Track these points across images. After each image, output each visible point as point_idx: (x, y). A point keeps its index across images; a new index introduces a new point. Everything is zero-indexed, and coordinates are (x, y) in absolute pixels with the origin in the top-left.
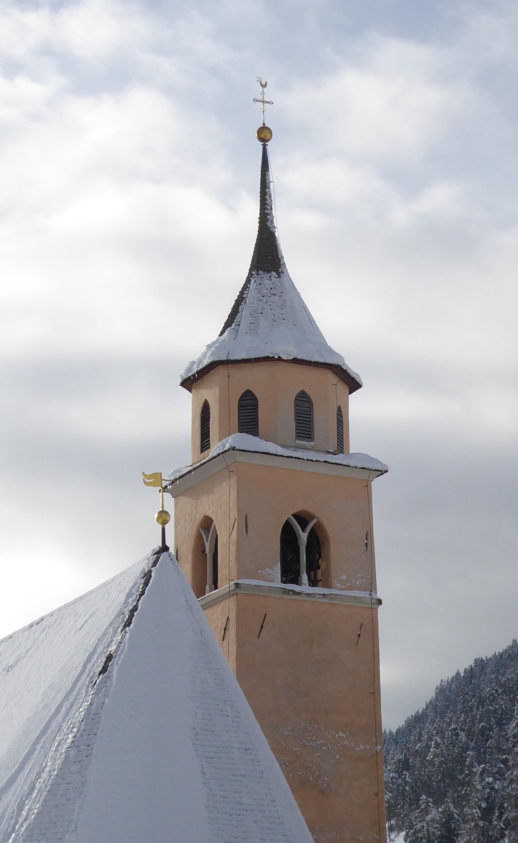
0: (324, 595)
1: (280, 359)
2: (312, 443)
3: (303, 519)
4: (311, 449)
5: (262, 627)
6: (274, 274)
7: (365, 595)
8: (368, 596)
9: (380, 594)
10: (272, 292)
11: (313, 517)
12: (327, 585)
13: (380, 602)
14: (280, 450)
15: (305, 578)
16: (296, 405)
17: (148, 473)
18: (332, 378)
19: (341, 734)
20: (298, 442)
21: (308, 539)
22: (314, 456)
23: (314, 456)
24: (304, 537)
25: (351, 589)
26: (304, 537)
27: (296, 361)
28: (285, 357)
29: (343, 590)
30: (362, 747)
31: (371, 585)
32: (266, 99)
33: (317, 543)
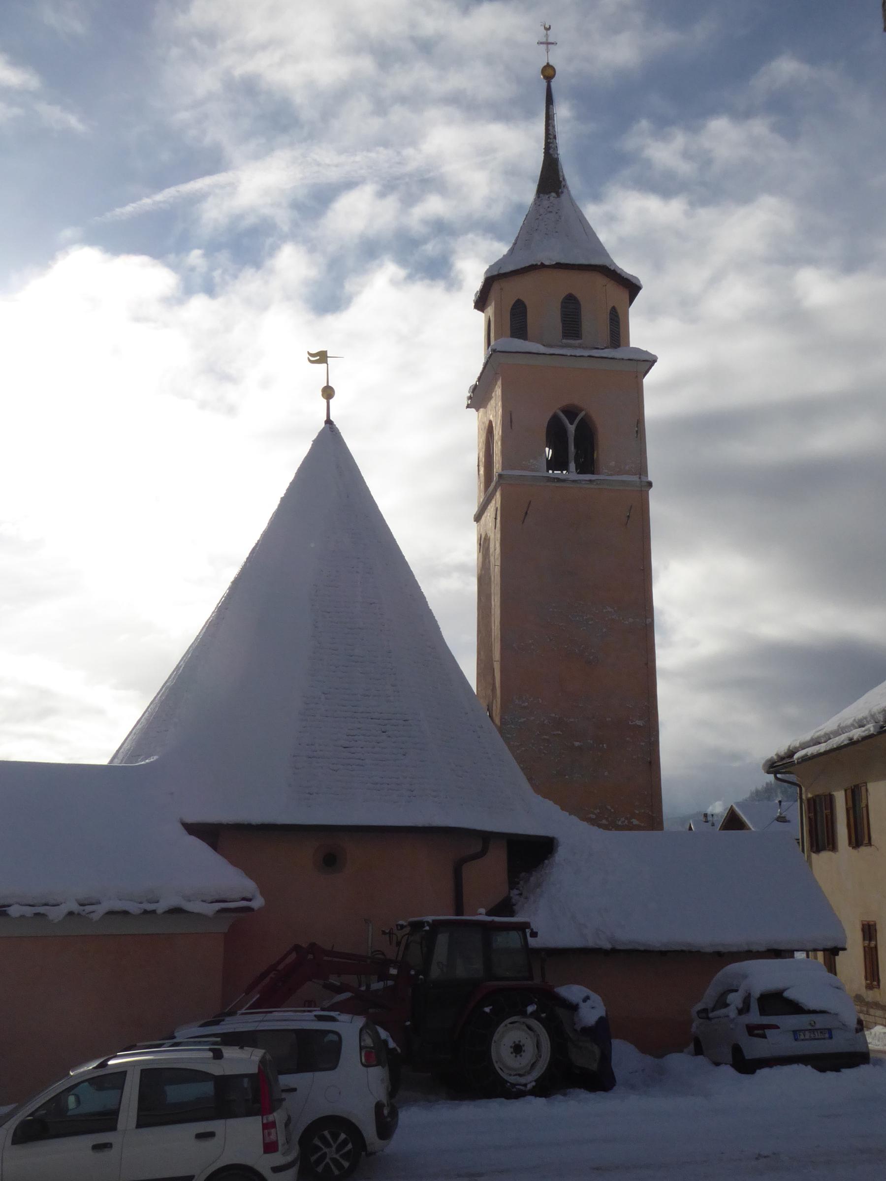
0: (590, 481)
1: (543, 266)
2: (579, 341)
3: (571, 412)
4: (580, 347)
5: (526, 513)
6: (553, 194)
7: (635, 478)
8: (638, 480)
9: (651, 477)
10: (549, 210)
11: (581, 410)
12: (598, 474)
13: (650, 484)
14: (542, 349)
15: (572, 466)
16: (562, 307)
17: (314, 352)
18: (600, 280)
19: (610, 609)
20: (564, 341)
21: (576, 431)
22: (578, 352)
23: (578, 352)
24: (571, 429)
25: (619, 473)
26: (571, 429)
27: (559, 266)
28: (547, 263)
29: (611, 475)
30: (631, 620)
31: (642, 469)
32: (550, 40)
33: (587, 437)
